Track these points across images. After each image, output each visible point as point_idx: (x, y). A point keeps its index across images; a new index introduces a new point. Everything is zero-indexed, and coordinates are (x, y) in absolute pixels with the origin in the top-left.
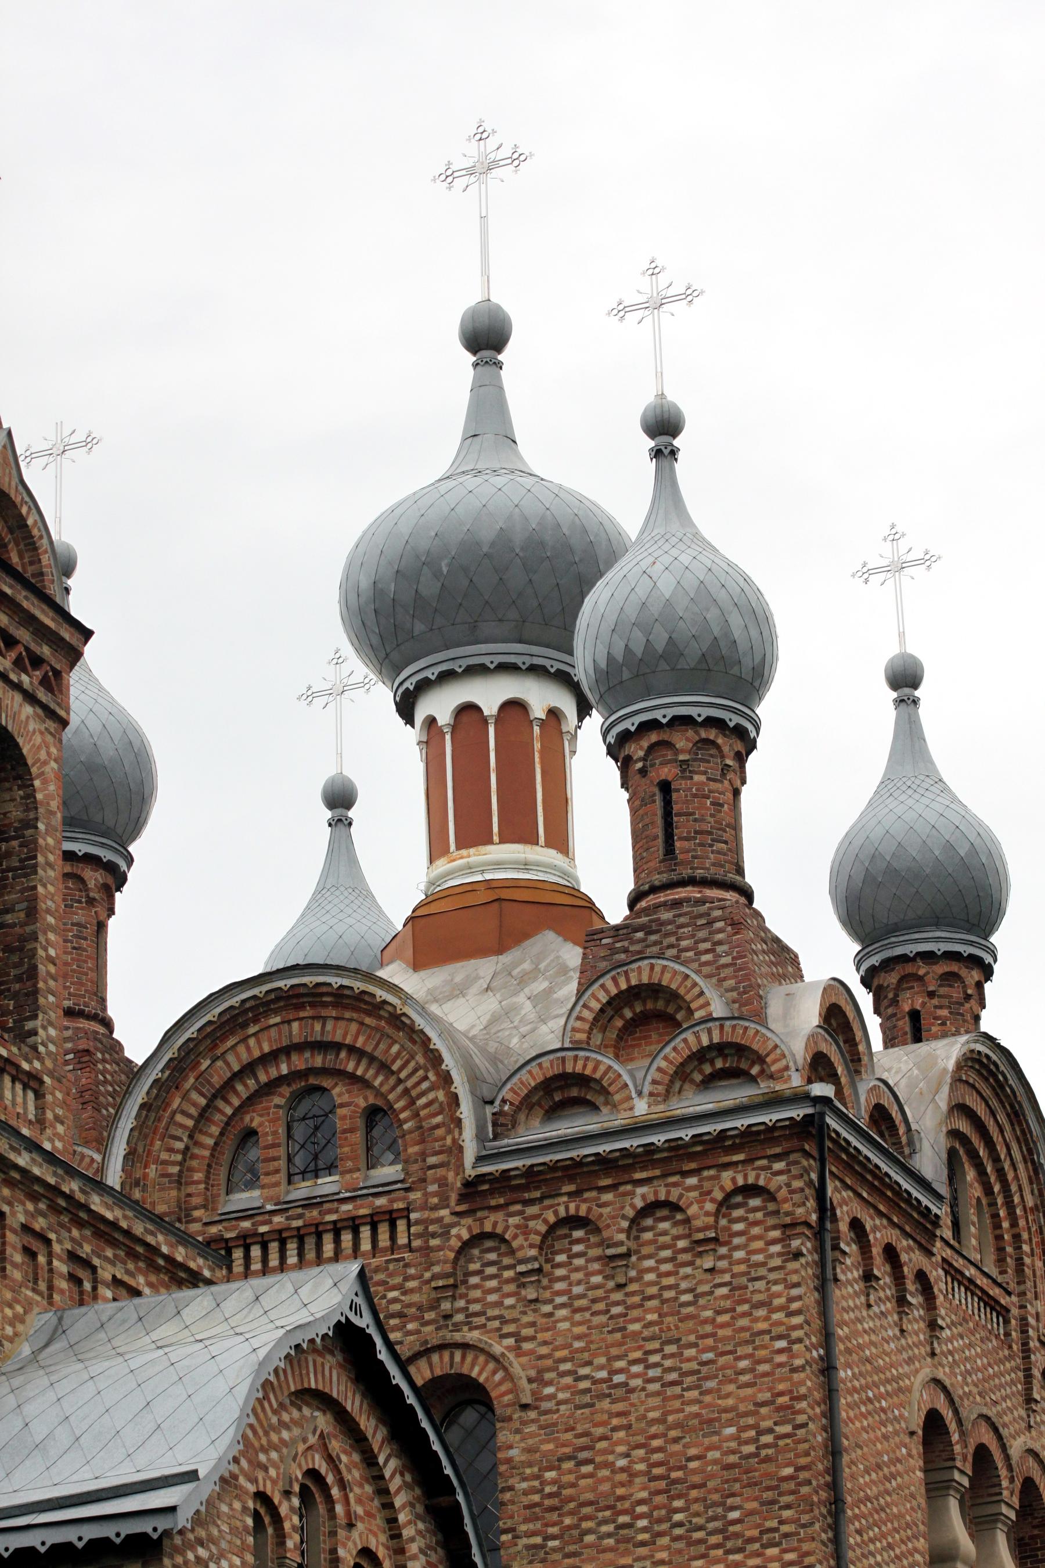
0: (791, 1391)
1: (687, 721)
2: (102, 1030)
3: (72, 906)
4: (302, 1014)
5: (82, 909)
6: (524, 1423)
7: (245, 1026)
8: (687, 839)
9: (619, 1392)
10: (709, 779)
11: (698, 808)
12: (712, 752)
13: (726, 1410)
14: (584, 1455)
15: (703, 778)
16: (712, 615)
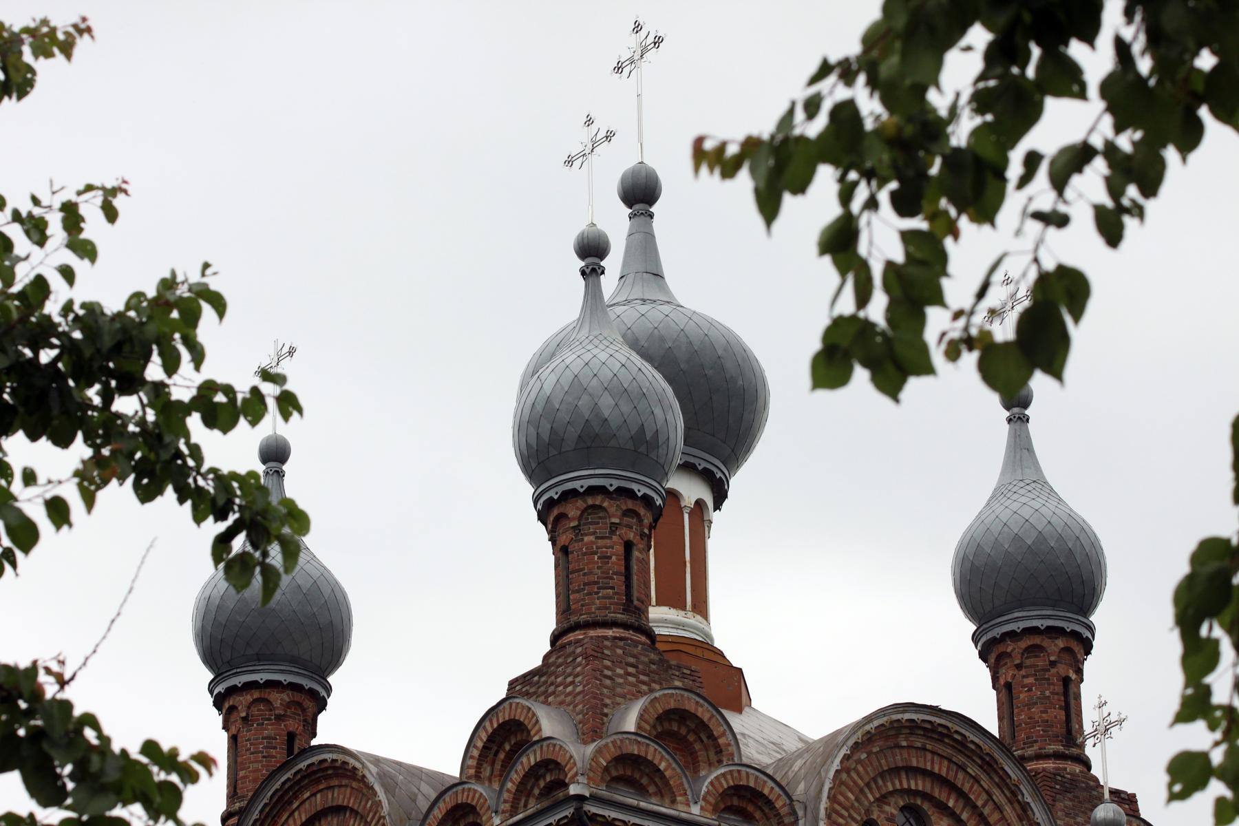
1: (573, 493)
2: (1078, 769)
4: (321, 787)
7: (290, 803)
8: (578, 591)
10: (597, 538)
15: (592, 538)
16: (584, 403)
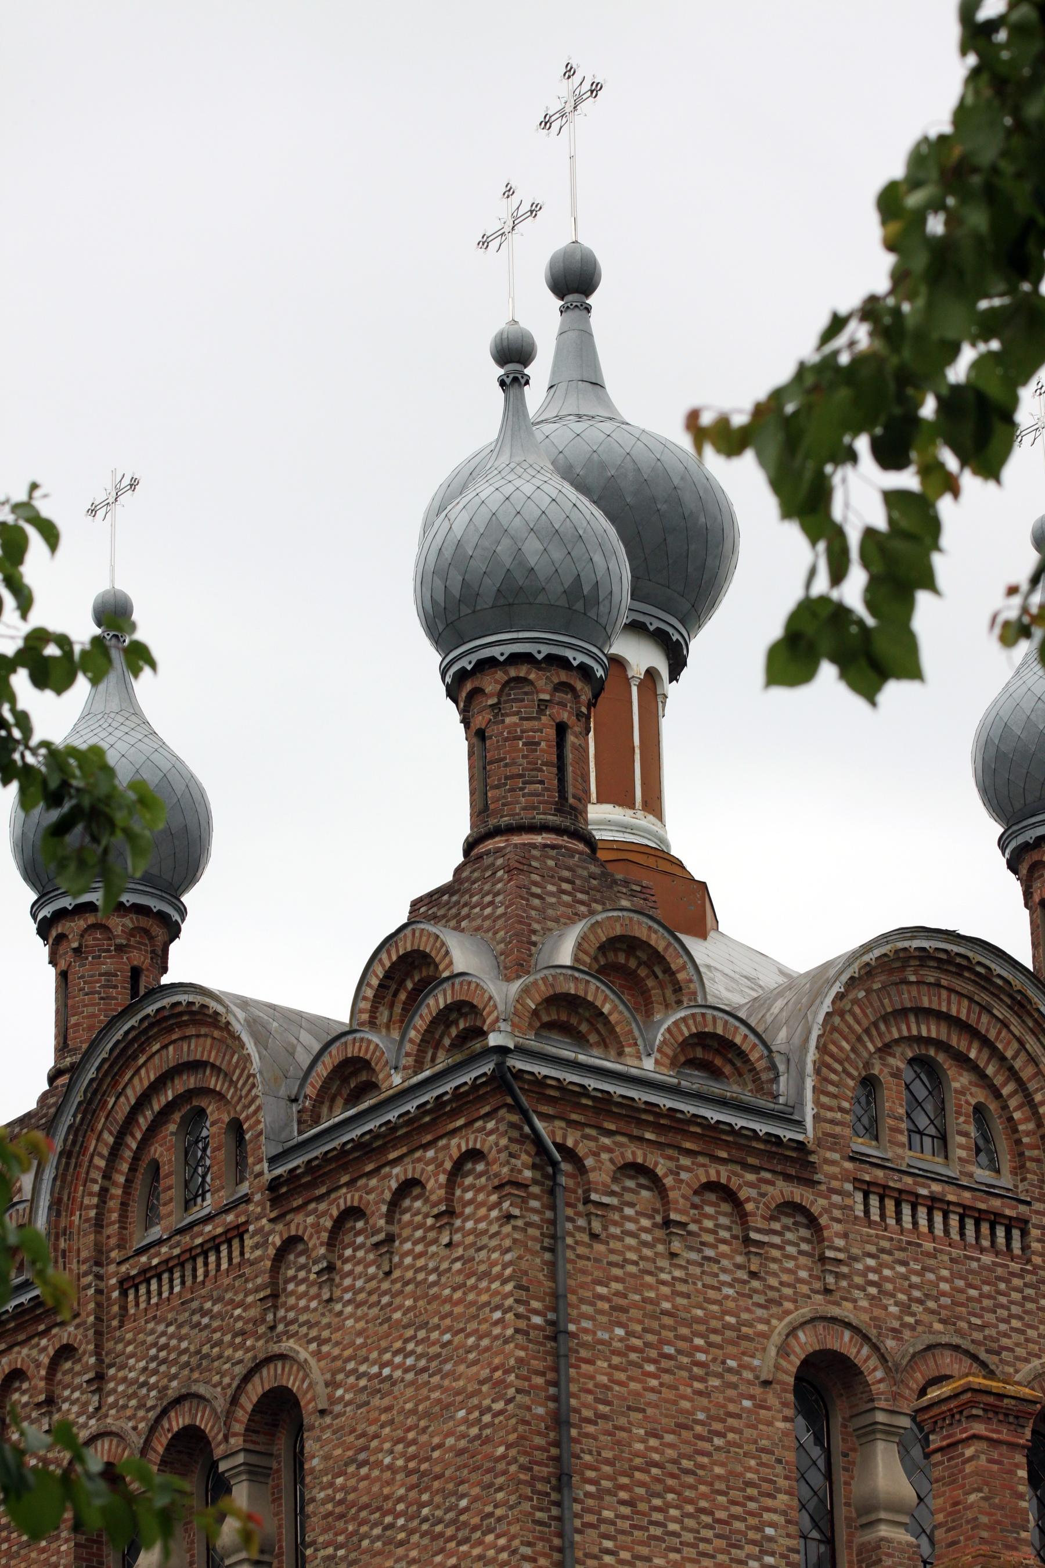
0: (503, 1365)
1: (490, 663)
3: (99, 957)
5: (111, 957)
6: (323, 1430)
8: (497, 787)
9: (385, 1386)
10: (521, 719)
11: (508, 752)
12: (526, 689)
13: (458, 1393)
14: (362, 1456)
16: (504, 548)
